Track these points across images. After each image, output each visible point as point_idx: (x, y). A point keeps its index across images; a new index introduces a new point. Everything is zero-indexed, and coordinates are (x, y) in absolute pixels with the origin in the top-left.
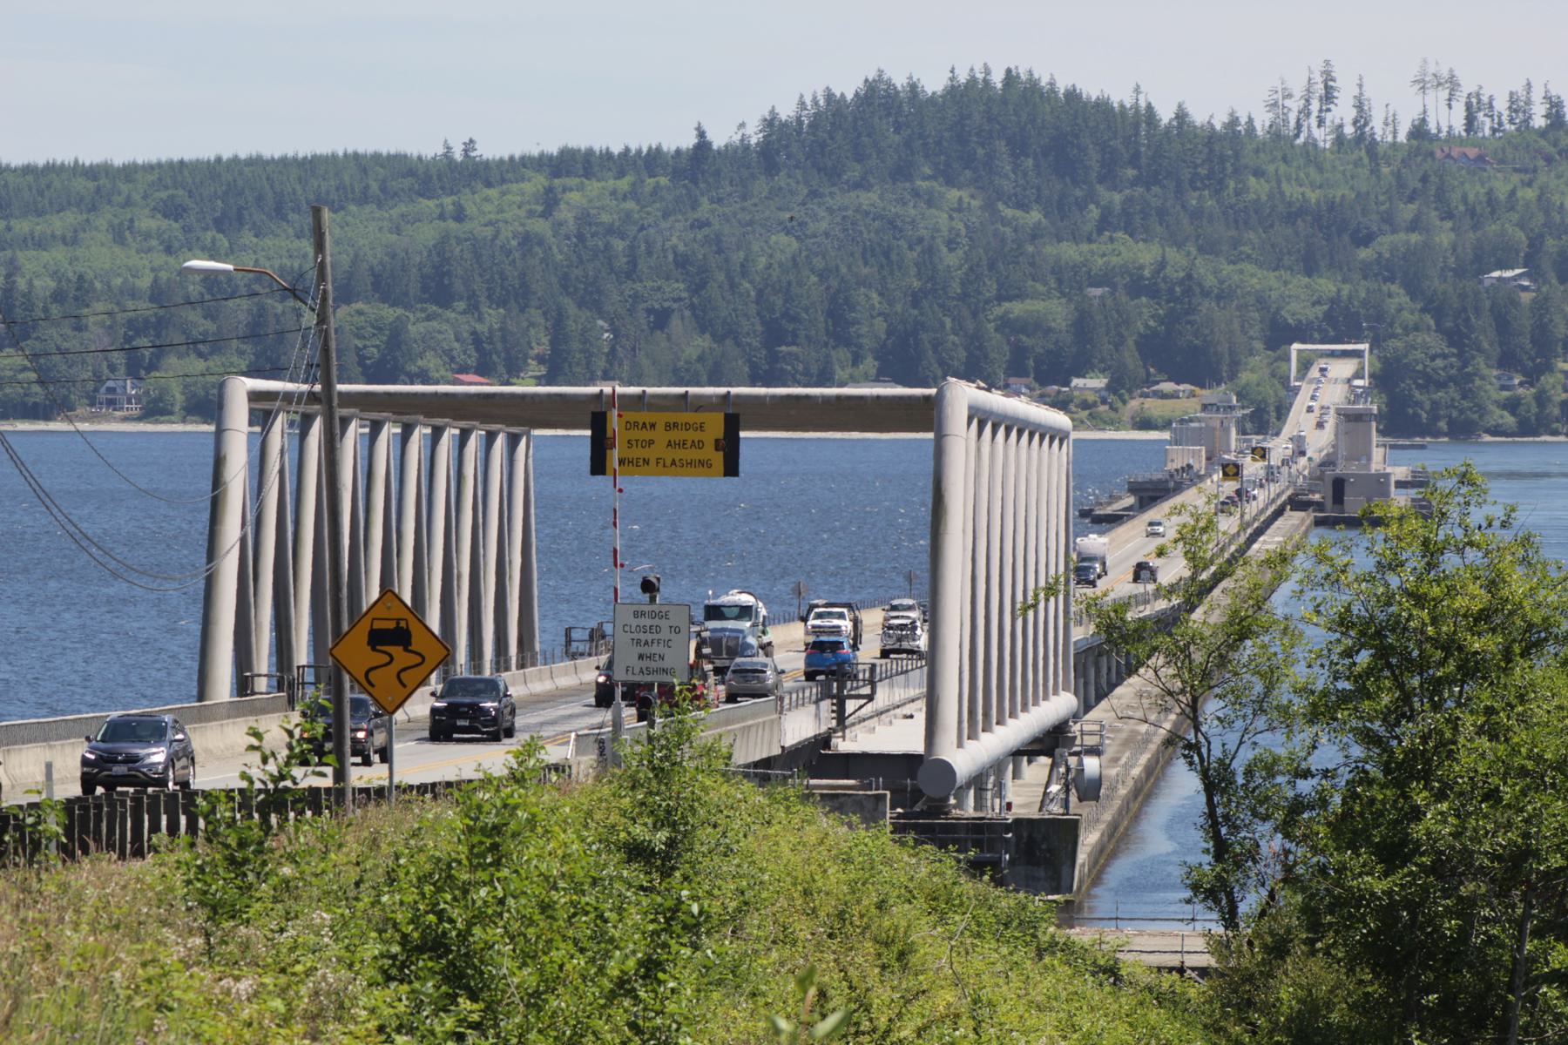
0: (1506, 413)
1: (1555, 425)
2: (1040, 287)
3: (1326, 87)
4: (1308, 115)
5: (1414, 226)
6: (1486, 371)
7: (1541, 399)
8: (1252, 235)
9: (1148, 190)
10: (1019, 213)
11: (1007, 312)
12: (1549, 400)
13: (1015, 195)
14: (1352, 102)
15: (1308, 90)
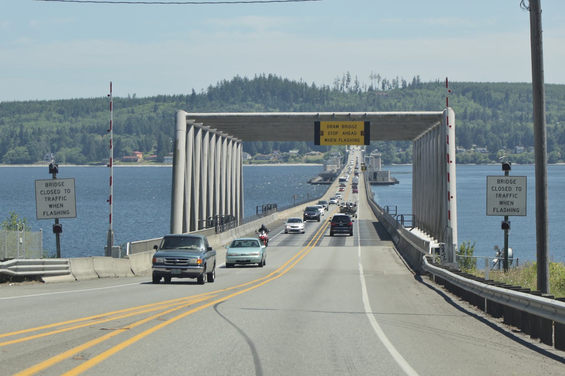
3: (348, 78)
7: (407, 154)
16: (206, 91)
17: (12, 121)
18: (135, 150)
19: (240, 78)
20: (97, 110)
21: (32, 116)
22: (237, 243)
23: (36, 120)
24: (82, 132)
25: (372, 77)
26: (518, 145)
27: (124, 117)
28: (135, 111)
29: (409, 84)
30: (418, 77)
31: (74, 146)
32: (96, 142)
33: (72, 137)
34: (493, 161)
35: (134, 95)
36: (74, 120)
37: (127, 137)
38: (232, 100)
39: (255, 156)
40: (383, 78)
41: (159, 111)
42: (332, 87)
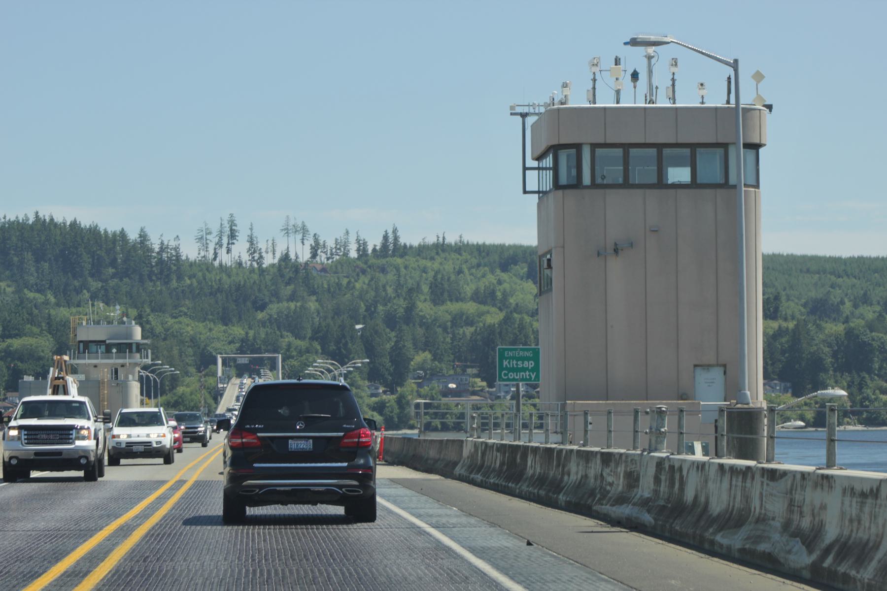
0: (375, 414)
1: (412, 422)
2: (36, 330)
3: (231, 230)
4: (221, 246)
5: (292, 298)
6: (360, 382)
7: (401, 402)
8: (187, 302)
9: (121, 280)
10: (37, 295)
11: (8, 347)
12: (408, 403)
13: (36, 284)
14: (247, 238)
15: (221, 232)
25: (286, 231)
29: (374, 250)
30: (395, 231)
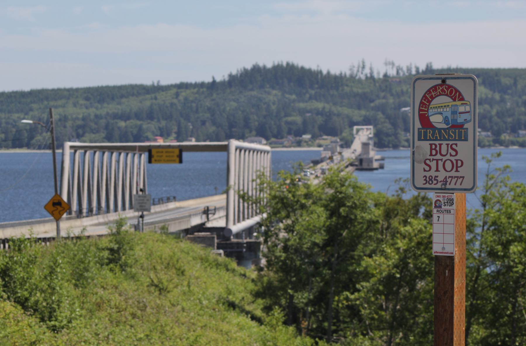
16: (227, 79)
17: (40, 108)
18: (157, 136)
19: (258, 66)
20: (122, 96)
21: (60, 102)
22: (468, 229)
23: (63, 106)
24: (106, 118)
25: (386, 64)
26: (520, 129)
27: (148, 103)
28: (158, 97)
31: (98, 131)
32: (119, 128)
33: (96, 124)
34: (497, 145)
35: (159, 82)
36: (99, 106)
37: (149, 123)
38: (250, 86)
39: (270, 141)
40: (397, 64)
41: (181, 98)
42: (348, 73)
